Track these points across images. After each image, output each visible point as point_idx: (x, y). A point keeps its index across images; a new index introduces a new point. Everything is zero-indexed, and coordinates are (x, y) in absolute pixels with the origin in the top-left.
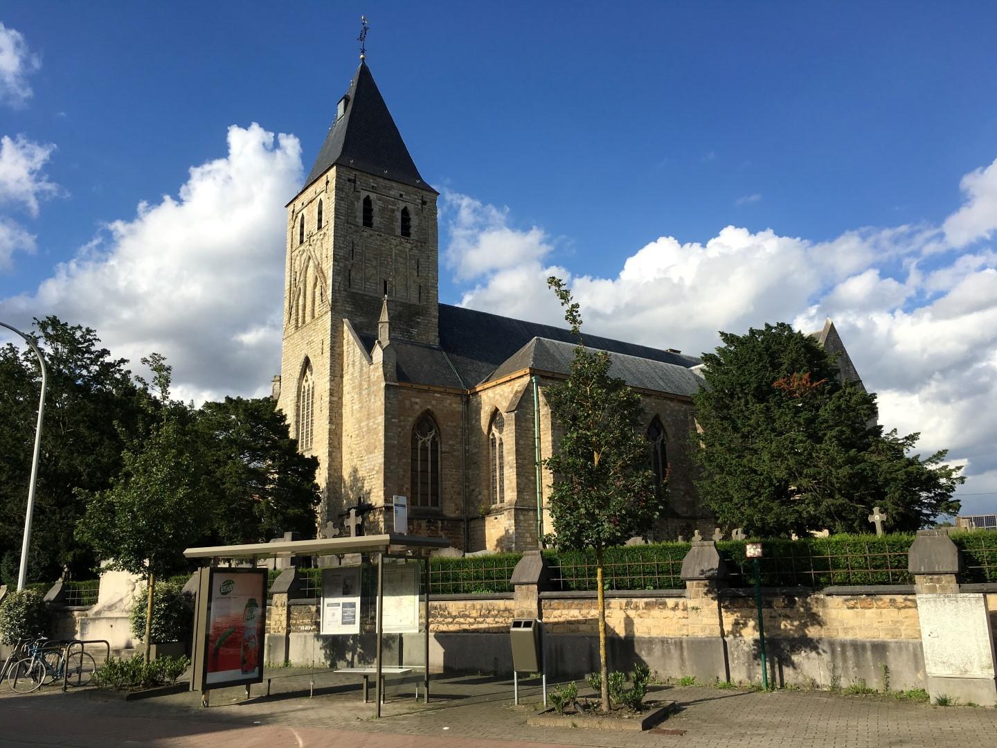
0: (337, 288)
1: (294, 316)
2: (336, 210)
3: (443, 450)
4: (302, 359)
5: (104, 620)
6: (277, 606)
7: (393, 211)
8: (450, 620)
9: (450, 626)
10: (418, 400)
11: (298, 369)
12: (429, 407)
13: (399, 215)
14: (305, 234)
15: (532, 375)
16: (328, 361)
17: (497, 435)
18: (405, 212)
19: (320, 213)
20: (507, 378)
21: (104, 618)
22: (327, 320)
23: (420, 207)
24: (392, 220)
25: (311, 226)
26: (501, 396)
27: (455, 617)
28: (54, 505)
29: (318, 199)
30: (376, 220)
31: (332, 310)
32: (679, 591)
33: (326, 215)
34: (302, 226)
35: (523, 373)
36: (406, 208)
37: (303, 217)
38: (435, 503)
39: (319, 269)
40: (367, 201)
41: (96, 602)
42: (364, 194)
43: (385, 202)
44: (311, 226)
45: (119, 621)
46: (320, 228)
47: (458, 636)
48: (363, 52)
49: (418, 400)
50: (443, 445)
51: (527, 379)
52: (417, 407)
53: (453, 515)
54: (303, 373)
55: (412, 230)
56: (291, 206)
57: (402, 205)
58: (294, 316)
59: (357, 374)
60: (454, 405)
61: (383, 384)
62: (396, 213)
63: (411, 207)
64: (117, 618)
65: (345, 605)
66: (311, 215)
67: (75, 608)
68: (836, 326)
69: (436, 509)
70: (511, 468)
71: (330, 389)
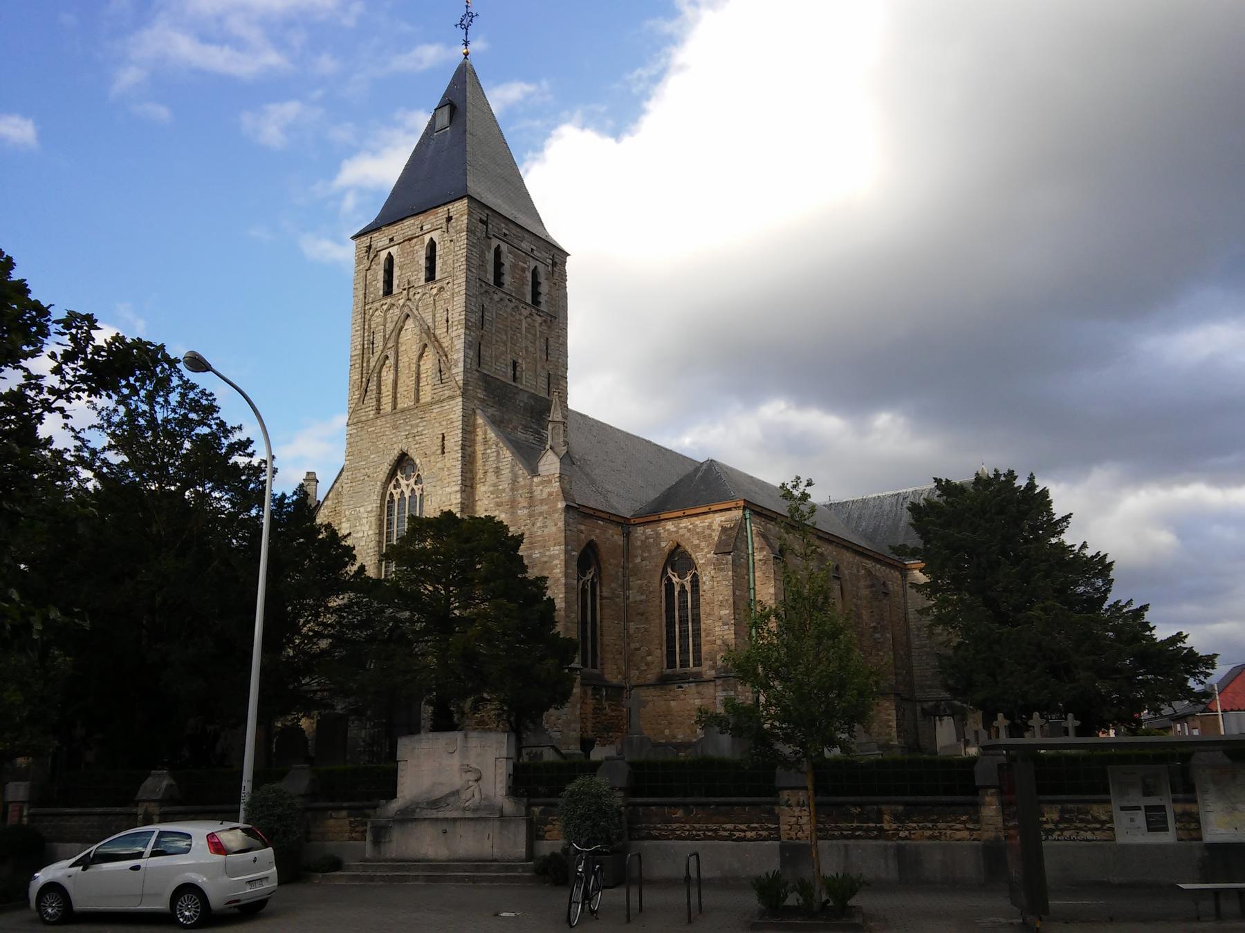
1: (372, 394)
2: (468, 259)
3: (605, 594)
4: (395, 453)
5: (426, 823)
6: (789, 806)
7: (523, 270)
10: (583, 527)
11: (385, 468)
12: (593, 537)
13: (529, 276)
14: (395, 282)
15: (745, 508)
16: (459, 464)
17: (675, 580)
18: (535, 273)
20: (705, 509)
21: (425, 819)
22: (456, 408)
25: (410, 270)
26: (689, 530)
30: (507, 279)
31: (463, 395)
32: (1103, 797)
33: (444, 263)
35: (732, 505)
38: (594, 666)
39: (429, 338)
40: (498, 252)
41: (393, 795)
42: (495, 243)
43: (516, 256)
45: (458, 824)
49: (583, 527)
50: (604, 589)
51: (737, 514)
52: (583, 536)
53: (615, 681)
54: (392, 475)
55: (543, 299)
56: (365, 240)
57: (532, 264)
58: (372, 394)
59: (505, 485)
60: (616, 537)
61: (561, 505)
63: (541, 268)
64: (455, 820)
65: (1148, 809)
69: (595, 671)
70: (725, 624)
71: (462, 503)
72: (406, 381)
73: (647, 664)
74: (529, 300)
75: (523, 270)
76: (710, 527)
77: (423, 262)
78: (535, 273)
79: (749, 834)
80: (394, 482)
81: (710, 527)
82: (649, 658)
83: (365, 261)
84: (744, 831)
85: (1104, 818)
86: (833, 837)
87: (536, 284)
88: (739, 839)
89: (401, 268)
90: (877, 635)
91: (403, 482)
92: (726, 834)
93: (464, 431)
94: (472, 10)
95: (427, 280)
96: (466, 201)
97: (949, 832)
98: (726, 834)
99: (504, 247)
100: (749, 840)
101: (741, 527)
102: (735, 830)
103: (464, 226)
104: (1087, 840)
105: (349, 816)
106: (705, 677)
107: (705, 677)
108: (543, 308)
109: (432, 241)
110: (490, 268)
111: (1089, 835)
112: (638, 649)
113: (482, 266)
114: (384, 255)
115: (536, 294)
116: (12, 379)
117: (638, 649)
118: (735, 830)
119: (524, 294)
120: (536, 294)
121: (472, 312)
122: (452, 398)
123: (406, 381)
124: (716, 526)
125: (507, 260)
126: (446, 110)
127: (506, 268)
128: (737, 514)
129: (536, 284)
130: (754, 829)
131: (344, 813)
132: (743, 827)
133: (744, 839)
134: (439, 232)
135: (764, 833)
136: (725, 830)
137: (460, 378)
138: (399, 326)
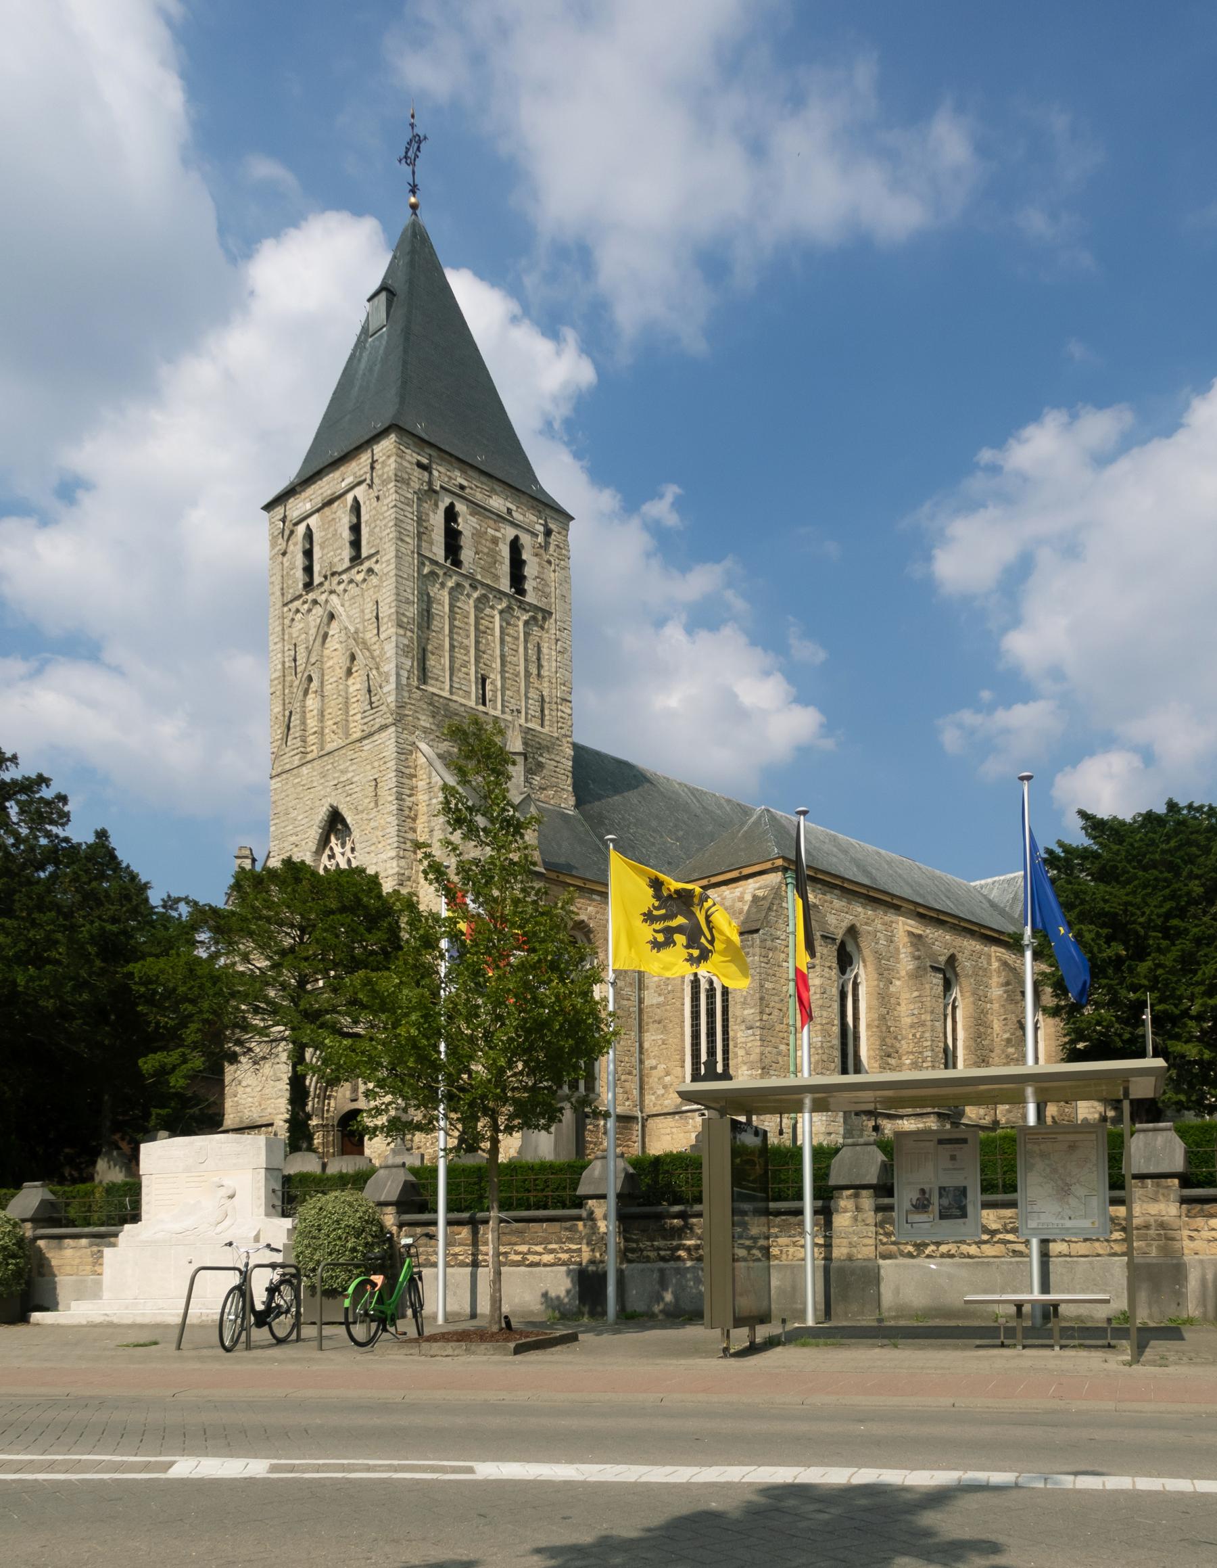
0: (404, 681)
4: (322, 813)
7: (495, 541)
8: (985, 1237)
9: (984, 1247)
11: (314, 833)
13: (505, 551)
18: (515, 547)
19: (356, 529)
22: (388, 741)
23: (541, 539)
24: (494, 556)
25: (332, 552)
27: (993, 1233)
28: (1126, 924)
29: (349, 497)
30: (467, 555)
33: (371, 533)
34: (308, 554)
36: (517, 538)
37: (309, 535)
44: (332, 552)
46: (356, 559)
47: (1002, 1263)
48: (413, 191)
55: (528, 586)
56: (279, 511)
57: (511, 532)
58: (295, 732)
62: (501, 545)
63: (525, 539)
66: (332, 534)
67: (1154, 1261)
68: (1103, 812)
72: (333, 709)
73: (665, 1087)
74: (505, 585)
75: (495, 541)
76: (741, 899)
77: (346, 535)
78: (515, 547)
79: (547, 1258)
80: (327, 852)
81: (741, 899)
82: (667, 1079)
83: (280, 541)
84: (540, 1254)
85: (994, 1226)
86: (648, 1260)
87: (517, 564)
88: (532, 1265)
89: (322, 548)
90: (1011, 1050)
91: (338, 850)
92: (518, 1258)
93: (400, 773)
94: (419, 130)
95: (352, 560)
96: (393, 437)
97: (791, 1250)
98: (518, 1258)
99: (460, 507)
100: (545, 1265)
101: (777, 894)
102: (529, 1252)
103: (391, 474)
104: (970, 1256)
105: (91, 1245)
106: (1176, 1181)
107: (1176, 1181)
108: (530, 598)
109: (355, 499)
110: (438, 536)
111: (973, 1250)
112: (655, 1068)
113: (422, 534)
114: (301, 529)
115: (517, 579)
116: (1211, 1002)
117: (655, 1068)
118: (529, 1252)
119: (496, 578)
120: (517, 579)
121: (408, 602)
122: (384, 728)
123: (333, 709)
124: (748, 897)
125: (467, 523)
126: (383, 295)
127: (466, 541)
128: (775, 878)
129: (517, 564)
130: (552, 1251)
131: (84, 1241)
132: (539, 1249)
133: (537, 1264)
134: (364, 487)
135: (565, 1256)
136: (517, 1253)
137: (391, 699)
138: (322, 633)
